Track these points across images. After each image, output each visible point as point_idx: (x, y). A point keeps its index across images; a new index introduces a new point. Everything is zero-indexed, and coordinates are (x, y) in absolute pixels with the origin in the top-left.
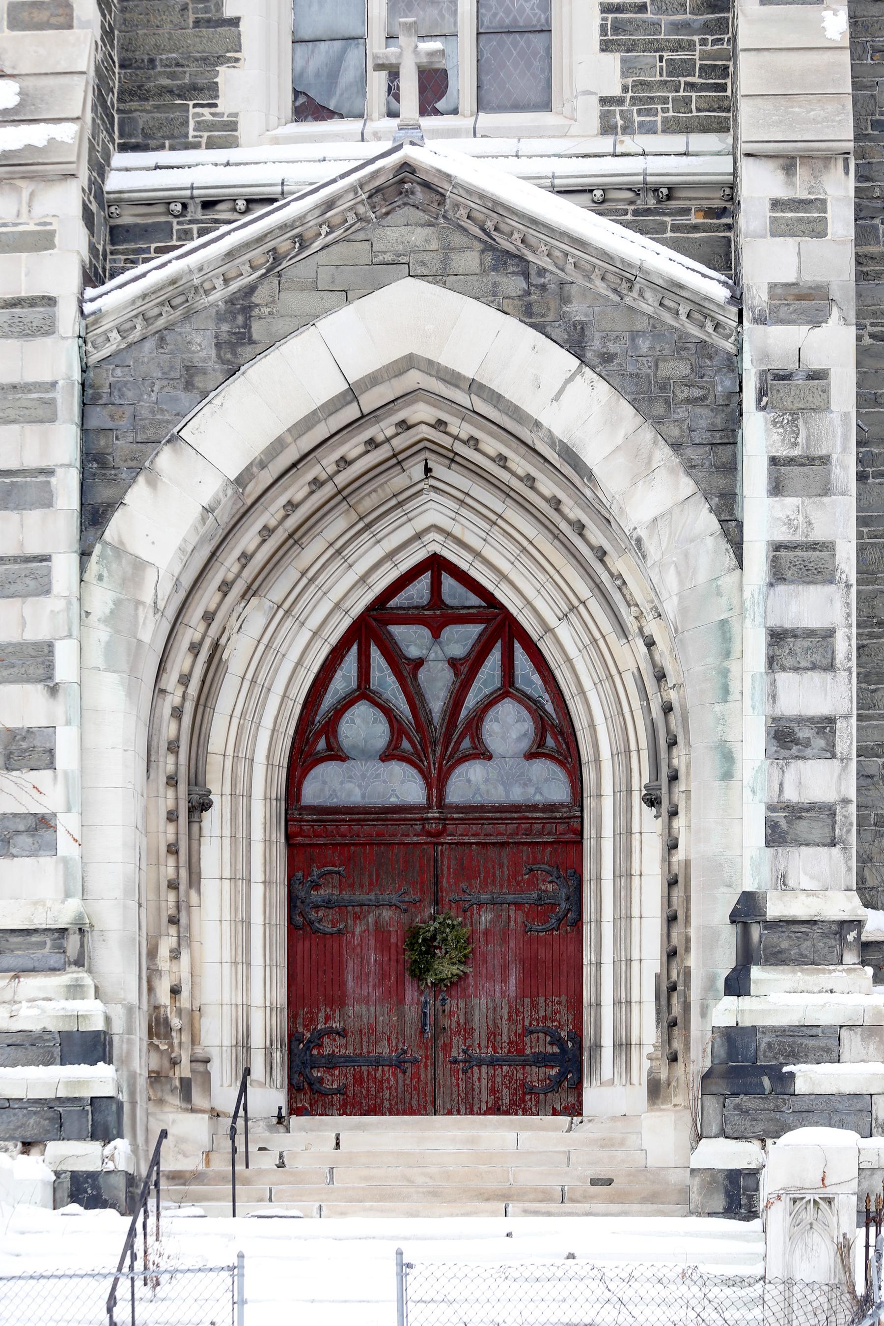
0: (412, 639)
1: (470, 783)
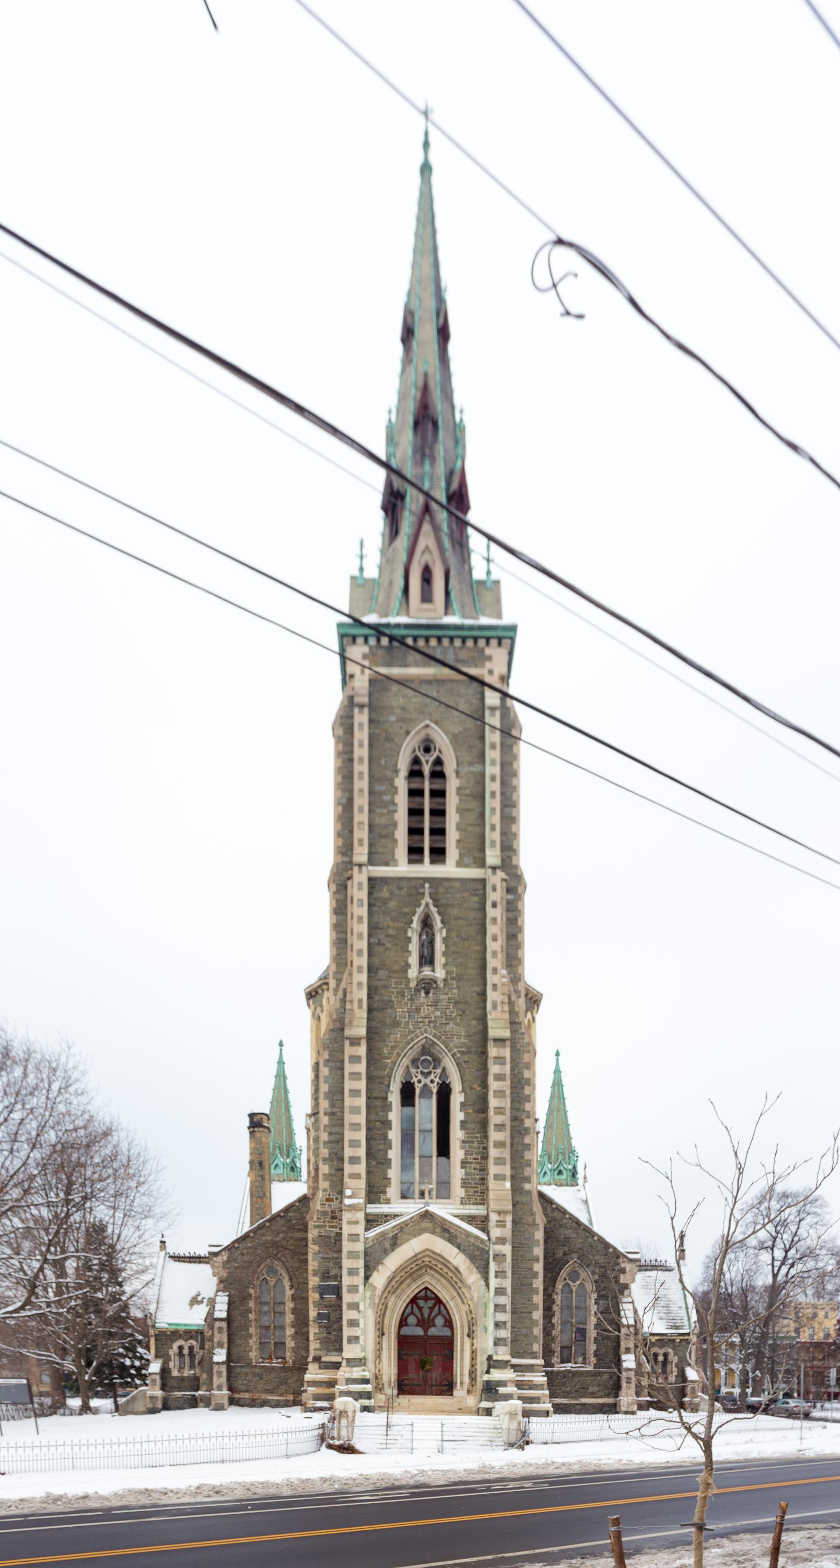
0: (421, 1303)
1: (433, 1331)
